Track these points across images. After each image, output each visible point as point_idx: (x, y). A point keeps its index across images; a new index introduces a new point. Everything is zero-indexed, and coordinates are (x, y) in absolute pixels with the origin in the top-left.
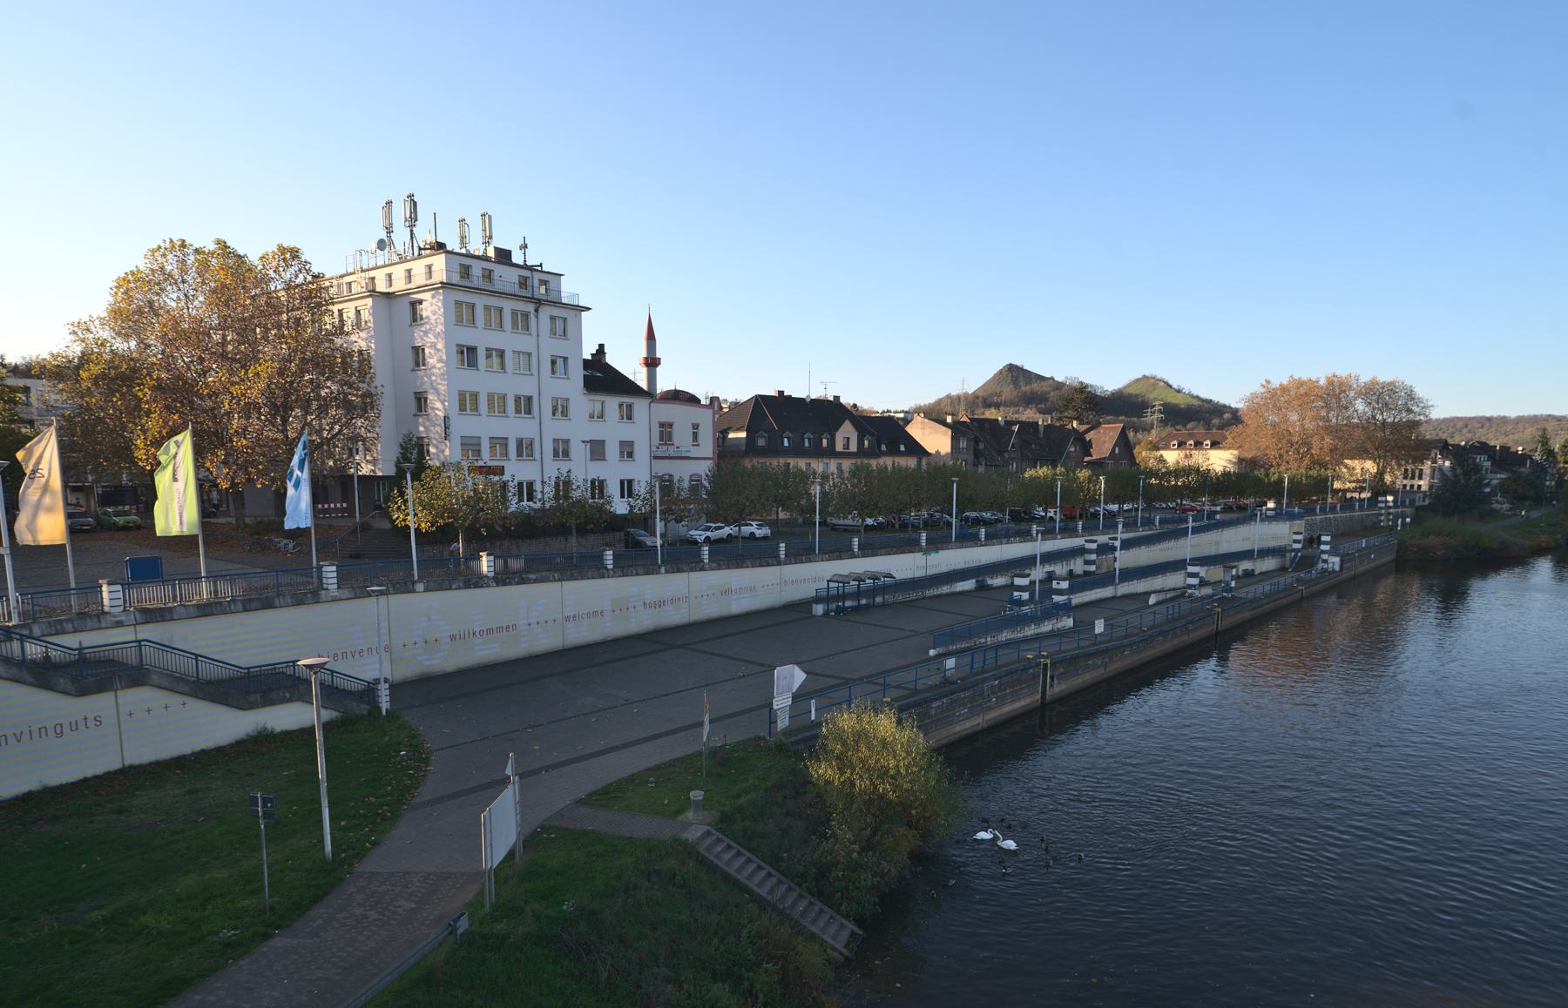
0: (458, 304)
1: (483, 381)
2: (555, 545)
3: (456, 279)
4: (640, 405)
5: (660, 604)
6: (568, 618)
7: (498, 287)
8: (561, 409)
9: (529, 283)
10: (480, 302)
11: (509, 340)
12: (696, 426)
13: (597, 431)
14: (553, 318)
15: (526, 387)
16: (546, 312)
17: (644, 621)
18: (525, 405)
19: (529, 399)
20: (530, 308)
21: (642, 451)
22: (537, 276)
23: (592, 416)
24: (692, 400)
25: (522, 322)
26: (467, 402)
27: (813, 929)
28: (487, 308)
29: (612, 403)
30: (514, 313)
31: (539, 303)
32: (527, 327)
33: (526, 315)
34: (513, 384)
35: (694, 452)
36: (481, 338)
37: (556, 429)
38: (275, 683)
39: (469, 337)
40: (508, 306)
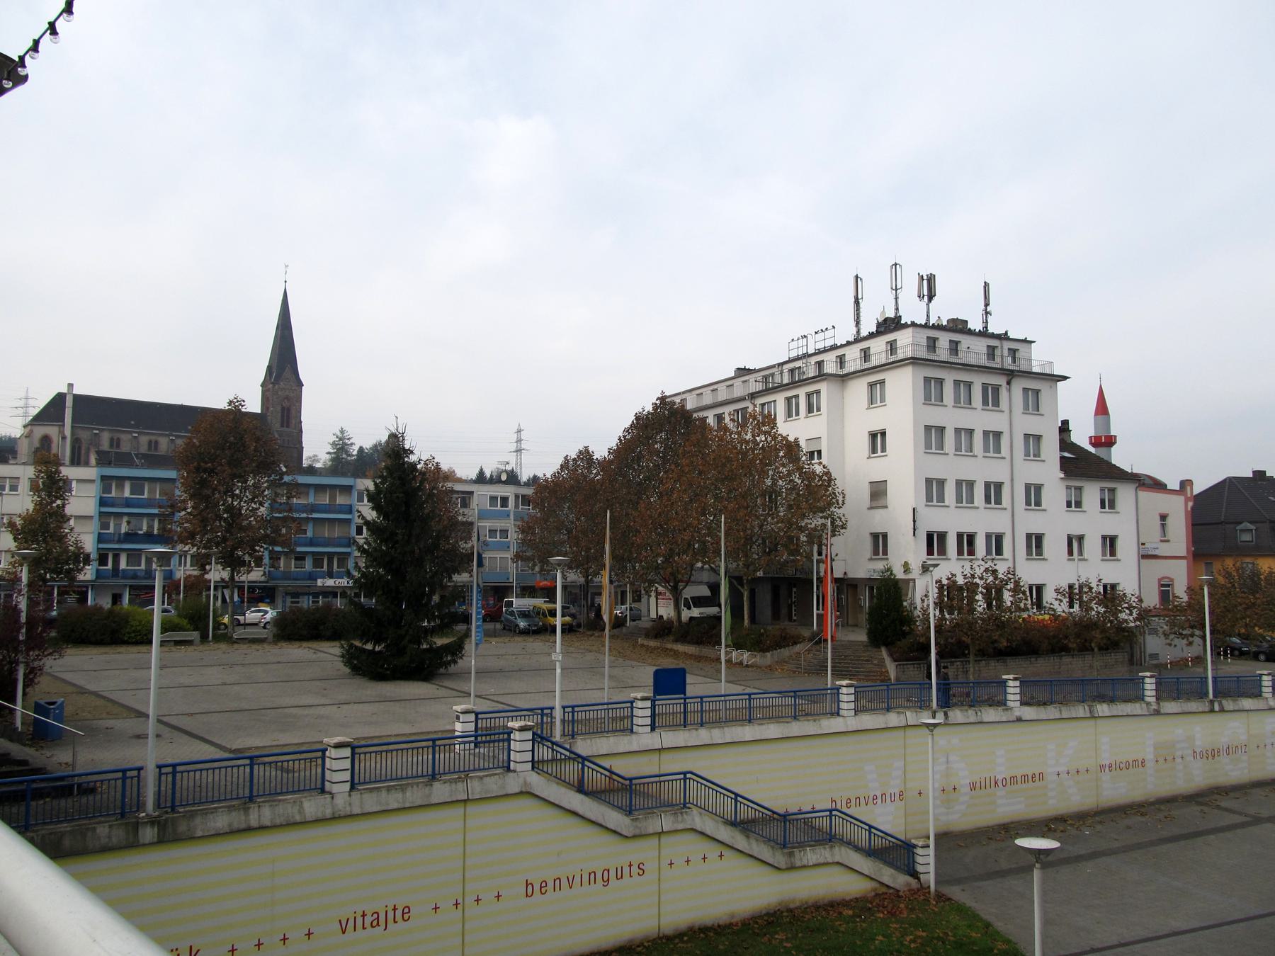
0: (927, 380)
1: (951, 468)
2: (1074, 666)
3: (923, 354)
4: (1125, 494)
5: (1213, 754)
6: (1102, 768)
7: (964, 358)
8: (1034, 495)
9: (998, 352)
10: (949, 377)
11: (980, 419)
12: (1163, 517)
13: (1076, 523)
14: (1026, 390)
15: (995, 470)
16: (1018, 386)
17: (1195, 777)
18: (994, 492)
19: (999, 486)
20: (1001, 381)
21: (1127, 548)
22: (1007, 345)
23: (1069, 504)
24: (1157, 485)
25: (992, 397)
26: (934, 489)
27: (513, 536)
28: (957, 383)
29: (1092, 493)
30: (985, 387)
31: (1011, 375)
32: (996, 403)
33: (996, 389)
34: (981, 469)
35: (1164, 550)
36: (950, 416)
37: (1031, 522)
38: (784, 832)
39: (936, 416)
40: (978, 381)
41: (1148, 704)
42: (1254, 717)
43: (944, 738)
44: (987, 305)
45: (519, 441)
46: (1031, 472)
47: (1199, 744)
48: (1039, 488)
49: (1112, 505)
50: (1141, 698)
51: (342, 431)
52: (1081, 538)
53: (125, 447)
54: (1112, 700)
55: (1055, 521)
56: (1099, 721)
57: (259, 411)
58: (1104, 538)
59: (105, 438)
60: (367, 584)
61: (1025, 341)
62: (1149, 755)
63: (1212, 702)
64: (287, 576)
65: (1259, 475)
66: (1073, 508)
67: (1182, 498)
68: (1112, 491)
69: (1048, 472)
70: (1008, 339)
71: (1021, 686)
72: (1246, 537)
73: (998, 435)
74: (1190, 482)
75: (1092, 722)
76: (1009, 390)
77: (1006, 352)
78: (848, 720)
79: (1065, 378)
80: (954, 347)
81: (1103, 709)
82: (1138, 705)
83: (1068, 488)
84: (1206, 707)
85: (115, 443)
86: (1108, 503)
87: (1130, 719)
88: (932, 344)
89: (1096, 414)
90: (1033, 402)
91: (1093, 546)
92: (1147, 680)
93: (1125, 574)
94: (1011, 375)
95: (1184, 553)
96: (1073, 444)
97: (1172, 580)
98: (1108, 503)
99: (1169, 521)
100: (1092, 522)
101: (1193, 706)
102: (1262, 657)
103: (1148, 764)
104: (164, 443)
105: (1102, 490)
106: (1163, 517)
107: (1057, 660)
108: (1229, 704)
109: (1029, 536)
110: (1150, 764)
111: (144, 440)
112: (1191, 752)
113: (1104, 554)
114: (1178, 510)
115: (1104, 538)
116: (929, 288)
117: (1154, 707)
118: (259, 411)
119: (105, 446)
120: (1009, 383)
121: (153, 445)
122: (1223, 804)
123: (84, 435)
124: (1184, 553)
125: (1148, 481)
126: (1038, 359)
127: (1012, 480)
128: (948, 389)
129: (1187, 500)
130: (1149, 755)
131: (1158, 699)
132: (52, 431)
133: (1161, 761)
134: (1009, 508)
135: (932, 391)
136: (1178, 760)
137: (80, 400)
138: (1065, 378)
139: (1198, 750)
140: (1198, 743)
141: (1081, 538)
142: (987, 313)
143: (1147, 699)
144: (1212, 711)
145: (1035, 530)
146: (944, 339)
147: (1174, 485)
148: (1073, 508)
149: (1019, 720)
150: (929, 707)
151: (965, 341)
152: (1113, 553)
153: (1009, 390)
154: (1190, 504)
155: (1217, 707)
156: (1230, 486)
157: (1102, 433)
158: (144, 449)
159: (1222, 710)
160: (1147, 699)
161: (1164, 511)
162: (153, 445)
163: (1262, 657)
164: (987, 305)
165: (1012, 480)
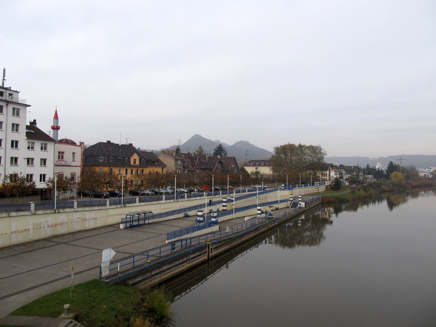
5: (55, 225)
6: (12, 233)
8: (15, 144)
12: (74, 153)
13: (30, 154)
14: (14, 109)
16: (11, 107)
17: (49, 232)
20: (4, 104)
21: (50, 163)
22: (8, 92)
23: (29, 148)
24: (73, 143)
29: (38, 145)
35: (73, 164)
41: (32, 211)
42: (70, 214)
44: (4, 77)
46: (15, 136)
47: (50, 223)
48: (17, 142)
49: (45, 149)
50: (30, 210)
51: (35, 121)
52: (33, 159)
54: (18, 211)
55: (22, 152)
56: (11, 218)
58: (41, 159)
61: (16, 91)
62: (31, 227)
63: (55, 210)
65: (109, 142)
66: (43, 150)
67: (80, 148)
68: (46, 144)
69: (21, 136)
70: (10, 90)
71: (35, 205)
72: (101, 161)
74: (83, 143)
75: (9, 218)
76: (7, 108)
77: (8, 95)
78: (164, 201)
79: (30, 106)
81: (13, 214)
82: (27, 212)
83: (28, 142)
84: (53, 211)
86: (44, 148)
87: (24, 217)
89: (54, 118)
90: (16, 112)
91: (37, 162)
92: (32, 204)
93: (36, 171)
94: (8, 103)
95: (80, 165)
96: (37, 128)
97: (63, 173)
98: (44, 148)
99: (75, 155)
100: (37, 154)
101: (172, 201)
102: (93, 196)
103: (30, 230)
105: (42, 144)
106: (74, 153)
107: (13, 199)
108: (61, 210)
109: (12, 158)
110: (31, 230)
112: (47, 225)
113: (41, 164)
114: (79, 151)
115: (41, 159)
117: (34, 212)
120: (7, 105)
122: (53, 240)
124: (80, 165)
125: (70, 142)
126: (21, 98)
127: (6, 138)
129: (82, 148)
131: (36, 210)
133: (36, 229)
134: (4, 148)
136: (42, 228)
138: (30, 106)
139: (50, 225)
140: (49, 223)
141: (33, 159)
142: (4, 79)
143: (32, 210)
144: (55, 213)
145: (15, 156)
147: (78, 144)
148: (43, 150)
149: (76, 211)
150: (53, 208)
152: (45, 164)
153: (7, 108)
154: (83, 150)
155: (57, 211)
156: (100, 145)
157: (55, 125)
159: (59, 212)
160: (32, 210)
161: (74, 152)
163: (93, 196)
164: (4, 77)
165: (6, 138)
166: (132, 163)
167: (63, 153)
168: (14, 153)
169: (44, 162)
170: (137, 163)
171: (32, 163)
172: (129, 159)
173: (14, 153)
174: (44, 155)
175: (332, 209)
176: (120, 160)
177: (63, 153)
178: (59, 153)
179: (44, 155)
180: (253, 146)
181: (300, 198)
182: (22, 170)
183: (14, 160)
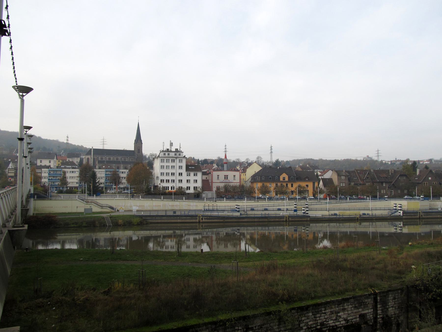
7: (170, 156)
13: (188, 178)
16: (178, 160)
18: (173, 174)
20: (175, 159)
23: (187, 175)
33: (174, 160)
34: (170, 171)
35: (234, 181)
39: (163, 164)
43: (130, 201)
45: (226, 149)
46: (180, 171)
53: (104, 159)
55: (185, 177)
57: (133, 150)
59: (100, 158)
60: (156, 187)
62: (161, 205)
64: (108, 185)
73: (174, 166)
80: (169, 154)
81: (154, 199)
85: (102, 158)
88: (165, 154)
104: (112, 158)
111: (107, 158)
116: (171, 144)
118: (133, 150)
119: (100, 159)
121: (110, 159)
123: (96, 157)
128: (165, 161)
130: (161, 205)
132: (89, 157)
135: (162, 161)
137: (94, 150)
146: (167, 153)
151: (170, 153)
158: (108, 160)
162: (110, 159)
166: (281, 179)
167: (227, 176)
168: (180, 178)
169: (196, 181)
170: (287, 179)
171: (190, 182)
172: (279, 177)
173: (180, 178)
174: (195, 178)
175: (221, 190)
176: (270, 178)
177: (227, 176)
178: (225, 176)
179: (195, 178)
180: (326, 160)
181: (386, 198)
182: (184, 185)
183: (181, 181)
